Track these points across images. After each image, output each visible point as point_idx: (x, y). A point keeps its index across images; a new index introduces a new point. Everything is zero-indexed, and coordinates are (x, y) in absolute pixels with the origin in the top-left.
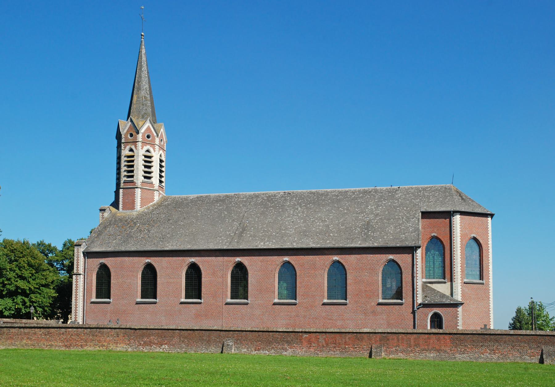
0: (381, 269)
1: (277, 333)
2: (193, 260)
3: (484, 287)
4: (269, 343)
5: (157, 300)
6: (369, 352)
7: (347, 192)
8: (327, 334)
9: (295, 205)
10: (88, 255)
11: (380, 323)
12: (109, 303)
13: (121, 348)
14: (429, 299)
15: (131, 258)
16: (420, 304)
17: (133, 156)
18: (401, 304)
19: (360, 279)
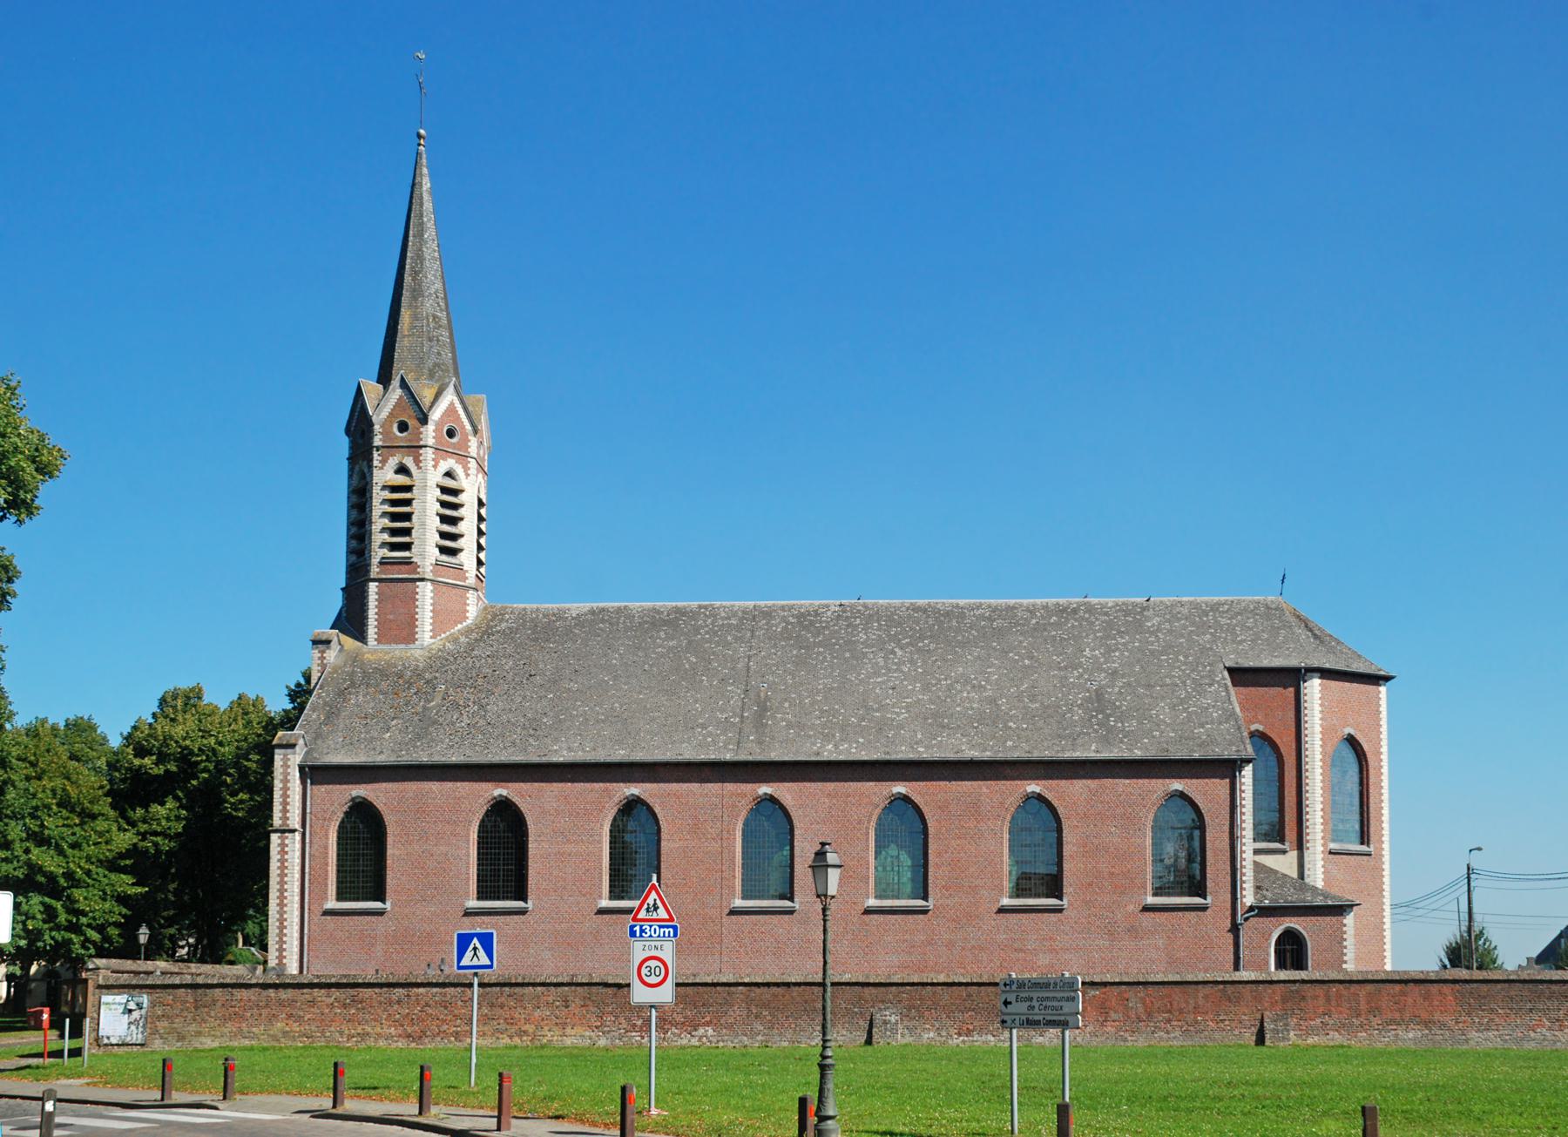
0: (1151, 816)
2: (634, 790)
8: (1150, 988)
10: (314, 773)
12: (380, 913)
13: (576, 1037)
14: (1269, 894)
15: (450, 784)
16: (1251, 909)
17: (408, 489)
18: (1204, 909)
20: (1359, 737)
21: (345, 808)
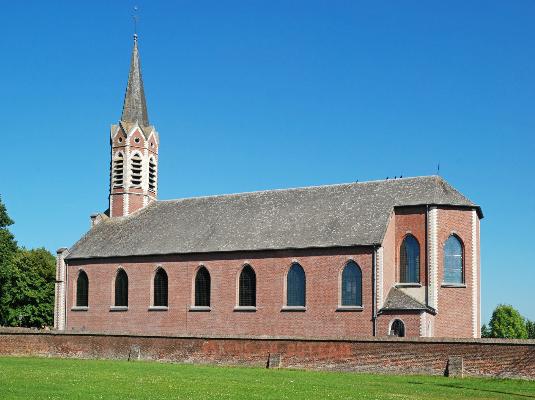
1: (180, 340)
2: (160, 265)
3: (466, 291)
4: (172, 350)
5: (128, 308)
6: (266, 361)
7: (326, 188)
8: (227, 341)
9: (271, 204)
10: (69, 262)
11: (337, 332)
13: (42, 354)
15: (106, 265)
16: (380, 311)
17: (122, 161)
18: (361, 311)
19: (318, 282)
20: (459, 234)
21: (78, 274)
